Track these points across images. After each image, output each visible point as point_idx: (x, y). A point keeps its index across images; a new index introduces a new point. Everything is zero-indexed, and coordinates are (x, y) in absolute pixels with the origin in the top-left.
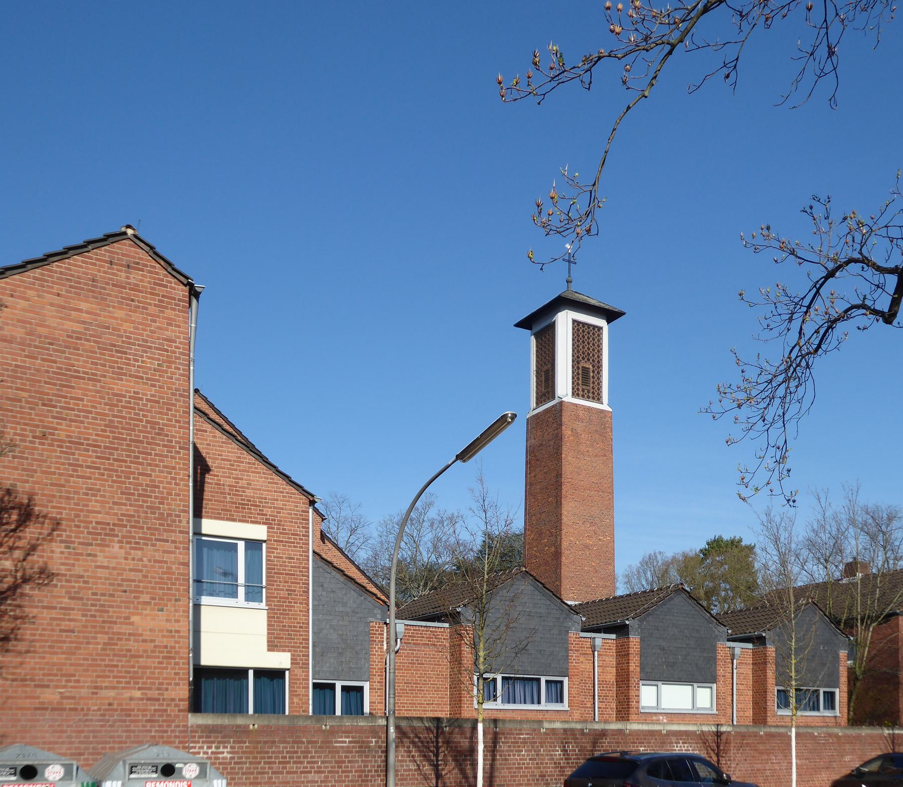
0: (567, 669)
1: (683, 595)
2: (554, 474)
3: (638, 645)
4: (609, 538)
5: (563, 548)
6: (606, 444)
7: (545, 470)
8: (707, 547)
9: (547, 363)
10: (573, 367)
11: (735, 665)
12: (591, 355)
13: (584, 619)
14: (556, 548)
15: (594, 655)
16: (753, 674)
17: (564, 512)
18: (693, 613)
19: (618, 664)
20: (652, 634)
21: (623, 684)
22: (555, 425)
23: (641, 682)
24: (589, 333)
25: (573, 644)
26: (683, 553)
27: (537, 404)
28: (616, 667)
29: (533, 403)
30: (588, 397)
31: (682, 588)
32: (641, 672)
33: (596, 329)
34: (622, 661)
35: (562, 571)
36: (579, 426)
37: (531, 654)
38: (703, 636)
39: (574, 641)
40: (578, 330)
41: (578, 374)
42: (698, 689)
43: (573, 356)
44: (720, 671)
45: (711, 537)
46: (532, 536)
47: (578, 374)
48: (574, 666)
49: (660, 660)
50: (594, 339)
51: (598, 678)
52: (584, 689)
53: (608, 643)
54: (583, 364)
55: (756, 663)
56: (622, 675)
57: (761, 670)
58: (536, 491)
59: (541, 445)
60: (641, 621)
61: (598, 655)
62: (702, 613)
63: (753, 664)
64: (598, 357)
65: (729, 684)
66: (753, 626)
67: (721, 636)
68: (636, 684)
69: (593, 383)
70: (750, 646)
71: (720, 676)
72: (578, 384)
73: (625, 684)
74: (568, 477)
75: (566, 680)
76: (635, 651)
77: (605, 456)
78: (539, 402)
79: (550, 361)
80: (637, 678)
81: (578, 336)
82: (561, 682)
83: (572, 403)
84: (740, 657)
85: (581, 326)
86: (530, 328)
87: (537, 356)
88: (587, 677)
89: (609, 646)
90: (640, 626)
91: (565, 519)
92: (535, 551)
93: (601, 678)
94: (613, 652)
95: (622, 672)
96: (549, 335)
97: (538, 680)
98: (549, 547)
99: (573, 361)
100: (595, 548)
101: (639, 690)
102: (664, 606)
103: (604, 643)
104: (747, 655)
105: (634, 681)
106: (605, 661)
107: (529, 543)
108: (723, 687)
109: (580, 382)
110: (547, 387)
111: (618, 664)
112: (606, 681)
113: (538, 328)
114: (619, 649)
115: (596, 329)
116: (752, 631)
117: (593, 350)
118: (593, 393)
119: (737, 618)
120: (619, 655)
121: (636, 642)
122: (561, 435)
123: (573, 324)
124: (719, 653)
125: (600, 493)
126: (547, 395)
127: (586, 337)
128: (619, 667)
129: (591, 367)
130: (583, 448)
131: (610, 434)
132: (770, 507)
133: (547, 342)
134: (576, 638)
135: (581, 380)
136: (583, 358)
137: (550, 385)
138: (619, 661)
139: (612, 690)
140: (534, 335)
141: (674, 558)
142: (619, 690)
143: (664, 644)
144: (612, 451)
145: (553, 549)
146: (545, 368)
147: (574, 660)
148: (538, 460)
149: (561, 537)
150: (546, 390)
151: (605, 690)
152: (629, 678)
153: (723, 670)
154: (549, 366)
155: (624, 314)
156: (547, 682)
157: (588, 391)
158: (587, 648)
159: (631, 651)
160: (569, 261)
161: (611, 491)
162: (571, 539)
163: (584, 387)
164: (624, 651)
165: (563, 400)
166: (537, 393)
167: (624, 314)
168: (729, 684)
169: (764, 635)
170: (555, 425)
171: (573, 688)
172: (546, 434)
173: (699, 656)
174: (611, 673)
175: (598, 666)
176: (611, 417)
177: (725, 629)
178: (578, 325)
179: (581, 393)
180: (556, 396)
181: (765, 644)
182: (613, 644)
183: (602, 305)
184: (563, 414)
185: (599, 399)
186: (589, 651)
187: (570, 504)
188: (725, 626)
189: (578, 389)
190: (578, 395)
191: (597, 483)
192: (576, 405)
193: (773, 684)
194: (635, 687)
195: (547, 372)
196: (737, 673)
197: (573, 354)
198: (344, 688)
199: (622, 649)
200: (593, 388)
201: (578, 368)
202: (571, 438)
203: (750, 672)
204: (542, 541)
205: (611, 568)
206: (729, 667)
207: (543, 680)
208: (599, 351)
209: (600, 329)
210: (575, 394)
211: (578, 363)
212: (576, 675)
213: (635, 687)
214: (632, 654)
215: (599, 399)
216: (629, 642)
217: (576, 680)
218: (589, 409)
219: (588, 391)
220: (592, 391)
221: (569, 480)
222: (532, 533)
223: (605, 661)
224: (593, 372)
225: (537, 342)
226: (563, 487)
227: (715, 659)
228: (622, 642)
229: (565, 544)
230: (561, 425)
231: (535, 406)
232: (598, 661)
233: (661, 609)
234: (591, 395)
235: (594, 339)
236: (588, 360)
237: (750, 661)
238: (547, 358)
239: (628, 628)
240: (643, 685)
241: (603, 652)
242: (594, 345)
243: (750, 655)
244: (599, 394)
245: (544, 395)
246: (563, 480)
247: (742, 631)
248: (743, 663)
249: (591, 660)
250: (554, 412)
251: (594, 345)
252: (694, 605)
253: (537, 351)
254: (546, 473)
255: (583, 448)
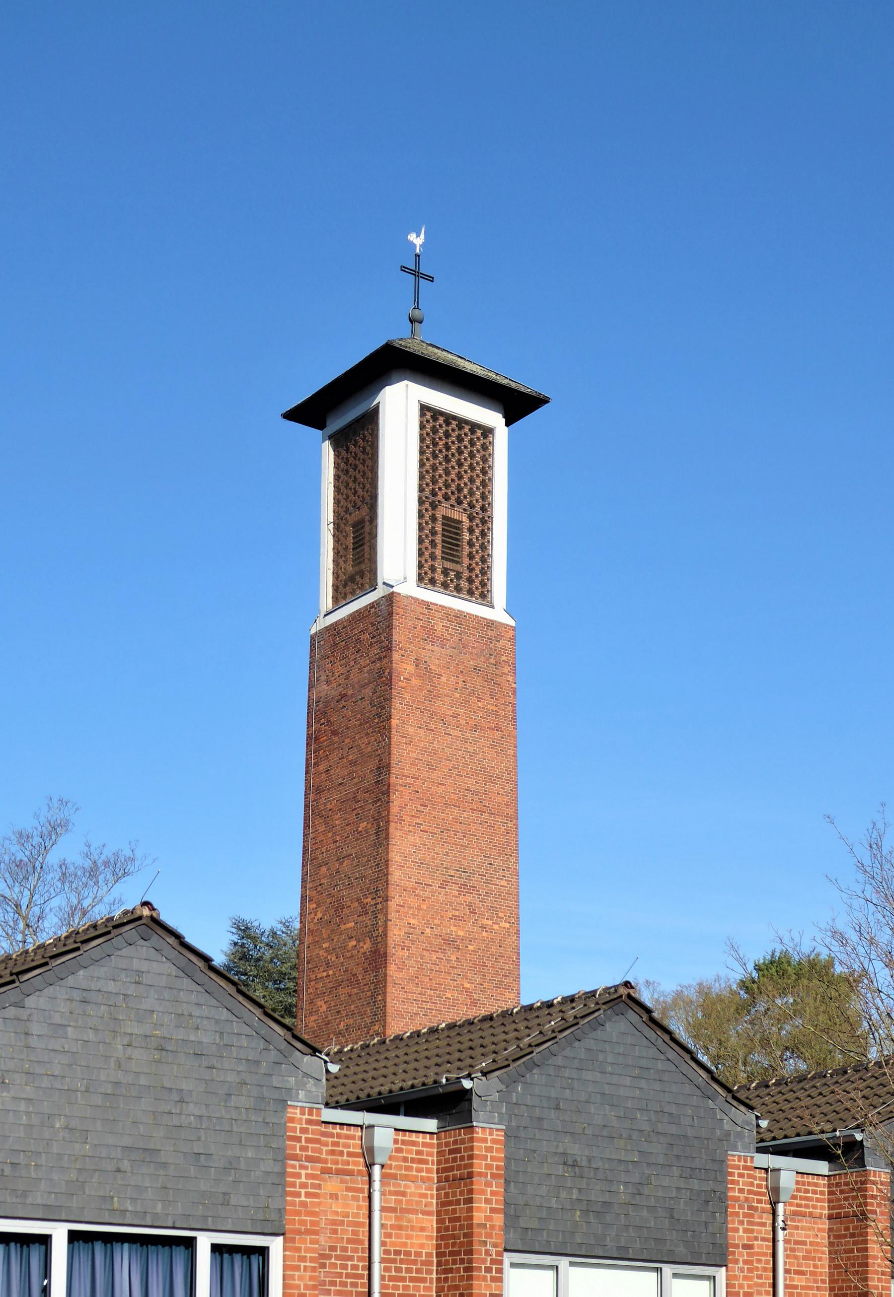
0: (281, 1211)
1: (631, 1015)
2: (372, 764)
3: (498, 1150)
4: (507, 925)
5: (391, 942)
6: (502, 701)
7: (351, 758)
8: (755, 975)
9: (359, 503)
10: (421, 516)
11: (780, 1218)
12: (466, 491)
13: (334, 1068)
14: (375, 943)
15: (370, 1175)
16: (831, 1244)
17: (395, 856)
18: (660, 1066)
19: (443, 1204)
20: (540, 1119)
21: (454, 1262)
22: (375, 650)
23: (508, 1258)
24: (460, 439)
25: (298, 1139)
26: (700, 984)
27: (335, 599)
28: (439, 1213)
29: (326, 599)
30: (458, 589)
31: (629, 996)
32: (507, 1227)
33: (479, 433)
34: (454, 1194)
35: (389, 1000)
36: (434, 656)
37: (165, 1165)
38: (690, 1132)
39: (304, 1131)
40: (434, 430)
41: (433, 533)
42: (677, 1282)
43: (421, 490)
44: (738, 1235)
45: (758, 953)
46: (319, 915)
47: (433, 533)
48: (303, 1204)
49: (563, 1194)
50: (472, 455)
51: (383, 1244)
52: (340, 1275)
53: (414, 1143)
54: (444, 510)
55: (838, 1216)
56: (454, 1237)
57: (852, 1235)
58: (329, 807)
59: (343, 696)
60: (510, 1083)
61: (384, 1176)
62: (684, 1068)
63: (830, 1217)
64: (484, 497)
65: (765, 1269)
66: (831, 1116)
67: (740, 1135)
68: (493, 1262)
69: (471, 556)
70: (822, 1167)
71: (737, 1246)
72: (433, 557)
73: (462, 1261)
74: (407, 772)
75: (276, 1246)
76: (489, 1167)
77: (498, 728)
78: (341, 595)
79: (368, 499)
80: (495, 1245)
81: (435, 444)
82: (263, 1252)
83: (416, 600)
84: (794, 1197)
85: (441, 420)
86: (320, 425)
87: (337, 489)
88: (349, 1241)
89: (419, 1153)
90: (504, 1096)
91: (396, 875)
92: (327, 950)
93: (393, 1244)
94: (429, 1171)
95: (454, 1229)
96: (363, 440)
97: (190, 1244)
98: (359, 941)
99: (421, 502)
100: (471, 948)
101: (500, 1280)
102: (577, 1044)
103: (404, 1142)
104: (814, 1192)
105: (487, 1252)
106: (403, 1194)
107: (311, 932)
108: (745, 1278)
109: (438, 552)
110: (359, 560)
111: (443, 1204)
112: (408, 1253)
113: (337, 423)
114: (447, 1161)
115: (479, 433)
116: (828, 1127)
117: (472, 480)
118: (470, 580)
119: (790, 1096)
120: (447, 1179)
121: (494, 1141)
122: (390, 674)
123: (422, 414)
124: (733, 1182)
125: (485, 816)
126: (358, 578)
127: (454, 449)
128: (446, 1212)
129: (464, 518)
130: (443, 707)
131: (510, 679)
132: (880, 825)
133: (362, 456)
134: (309, 1122)
135: (439, 546)
136: (446, 498)
137: (367, 556)
138: (447, 1195)
139: (423, 1280)
140: (330, 438)
141: (679, 995)
142: (446, 1279)
143: (575, 1150)
144: (514, 718)
145: (367, 946)
146: (356, 516)
147: (303, 1185)
148: (335, 733)
149: (386, 914)
150: (357, 569)
151: (403, 1279)
152: (471, 1243)
153: (745, 1231)
154: (365, 511)
155: (544, 401)
156: (217, 1249)
157: (459, 576)
158: (350, 1154)
159: (479, 1166)
160: (417, 274)
161: (511, 812)
162: (412, 921)
163: (448, 565)
164: (459, 1168)
165: (395, 589)
166: (336, 575)
167: (544, 401)
168: (765, 1269)
169: (859, 1137)
170: (375, 650)
171: (297, 1268)
172: (355, 670)
173: (679, 1189)
174: (422, 1229)
175: (383, 1209)
176: (513, 640)
177: (751, 1116)
178: (435, 419)
179: (439, 577)
180: (380, 581)
181: (861, 1162)
182: (430, 1145)
183: (494, 376)
184: (396, 623)
185: (483, 596)
186: (356, 1164)
187: (411, 838)
188: (751, 1108)
189: (433, 569)
190: (433, 582)
191: (477, 792)
192: (428, 605)
193: (883, 1273)
194: (489, 1270)
195: (358, 526)
196: (786, 1241)
197: (420, 486)
198: (217, 1249)
199: (455, 1159)
200: (471, 570)
201: (434, 519)
202: (415, 682)
203: (823, 1239)
204: (343, 927)
205: (512, 996)
206: (763, 1225)
207: (204, 1243)
208: (484, 484)
209: (488, 432)
210: (425, 577)
211: (434, 506)
212: (308, 1232)
213: (489, 1270)
214: (480, 1174)
215: (483, 596)
216: (472, 1140)
217: (305, 1244)
218: (459, 617)
219: (459, 576)
220: (466, 574)
221: (409, 780)
222: (318, 905)
223: (403, 1194)
224: (471, 531)
225: (337, 455)
226: (393, 797)
227: (723, 1198)
228: (455, 1142)
229: (395, 934)
230: (389, 649)
231: (330, 606)
232: (383, 1194)
233: (568, 1052)
234: (464, 584)
235: (472, 455)
236: (460, 502)
237: (822, 1208)
238: (360, 492)
239: (470, 1100)
240: (513, 1265)
241: (399, 1168)
242: (472, 468)
243: (822, 1193)
244: (483, 584)
245: (352, 579)
246: (393, 779)
247: (800, 1129)
248: (803, 1215)
249: (361, 1190)
250: (372, 620)
251: (472, 468)
252: (664, 1047)
253: (337, 477)
254: (353, 763)
255: (443, 707)
